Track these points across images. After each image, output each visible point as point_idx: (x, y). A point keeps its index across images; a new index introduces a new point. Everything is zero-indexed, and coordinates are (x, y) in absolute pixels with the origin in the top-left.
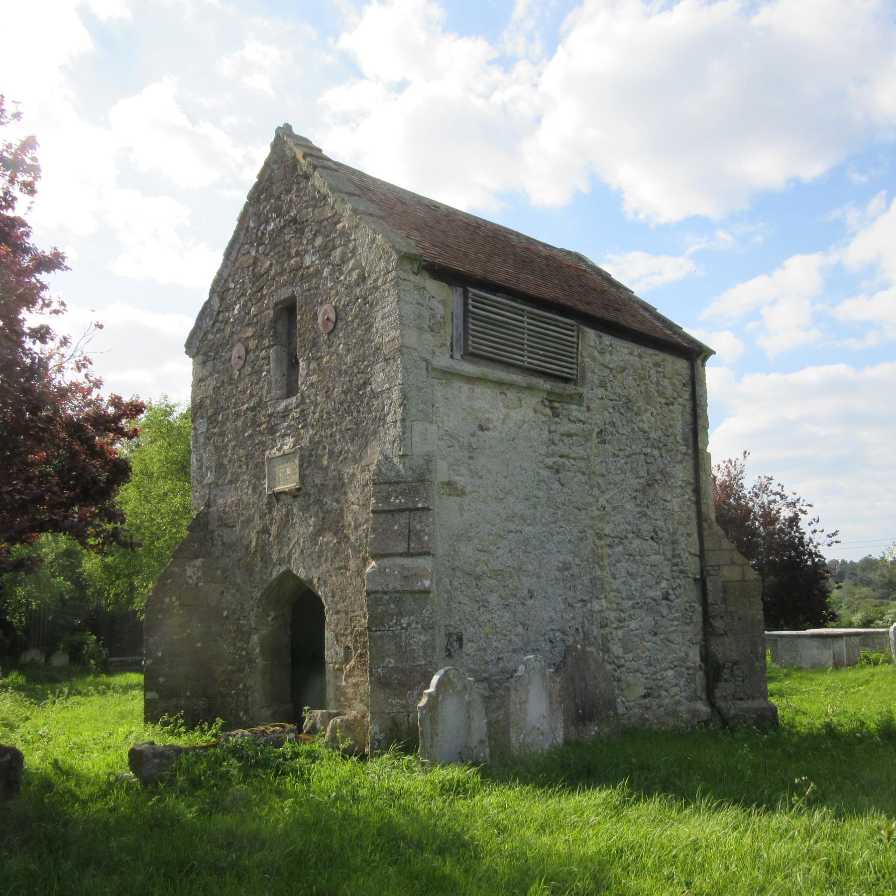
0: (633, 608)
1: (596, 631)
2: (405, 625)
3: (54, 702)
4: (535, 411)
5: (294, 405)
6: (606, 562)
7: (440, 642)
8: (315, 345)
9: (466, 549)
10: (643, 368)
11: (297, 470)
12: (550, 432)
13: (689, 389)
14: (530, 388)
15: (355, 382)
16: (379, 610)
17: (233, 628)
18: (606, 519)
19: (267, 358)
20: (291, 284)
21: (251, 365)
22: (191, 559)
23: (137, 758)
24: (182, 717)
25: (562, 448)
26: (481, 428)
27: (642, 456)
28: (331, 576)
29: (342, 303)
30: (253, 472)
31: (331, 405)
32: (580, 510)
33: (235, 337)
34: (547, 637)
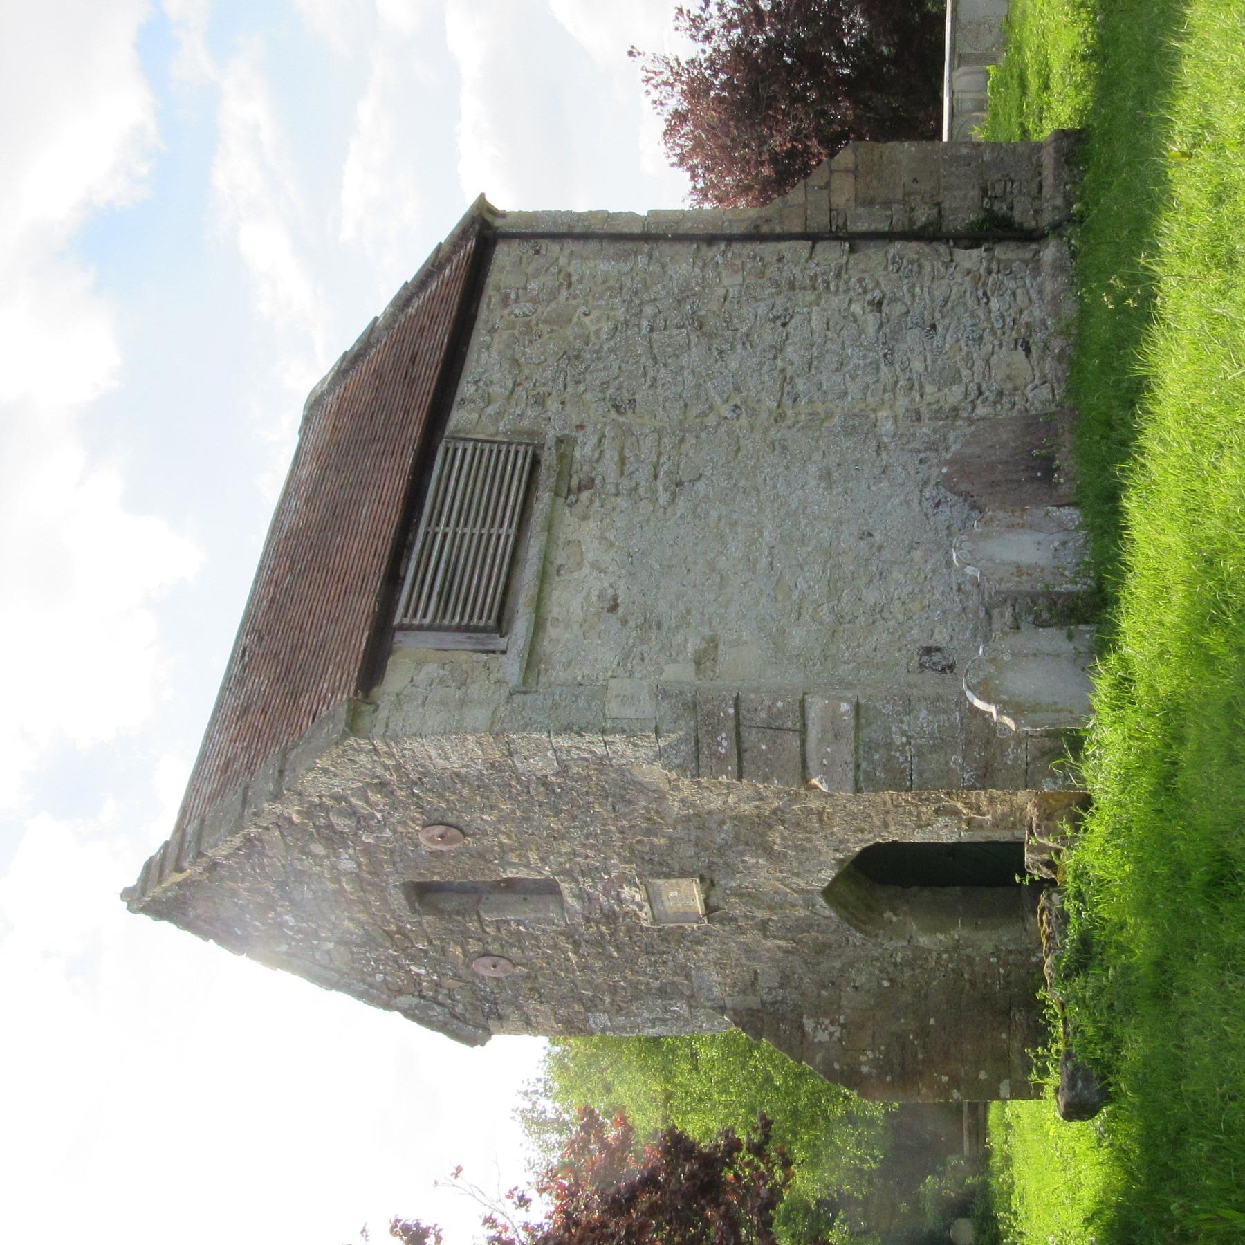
0: (892, 364)
1: (925, 430)
2: (904, 740)
3: (1021, 1234)
4: (585, 518)
5: (573, 885)
6: (820, 407)
7: (930, 683)
8: (481, 856)
9: (797, 637)
10: (511, 326)
11: (673, 881)
12: (617, 494)
13: (544, 244)
14: (549, 527)
15: (541, 798)
16: (883, 776)
17: (908, 973)
18: (752, 404)
19: (498, 925)
20: (384, 889)
21: (507, 947)
22: (804, 1034)
23: (1076, 1110)
24: (1034, 1050)
25: (644, 475)
26: (614, 608)
27: (655, 335)
28: (832, 834)
29: (418, 815)
30: (673, 944)
31: (575, 833)
32: (739, 449)
33: (462, 971)
34: (930, 511)
